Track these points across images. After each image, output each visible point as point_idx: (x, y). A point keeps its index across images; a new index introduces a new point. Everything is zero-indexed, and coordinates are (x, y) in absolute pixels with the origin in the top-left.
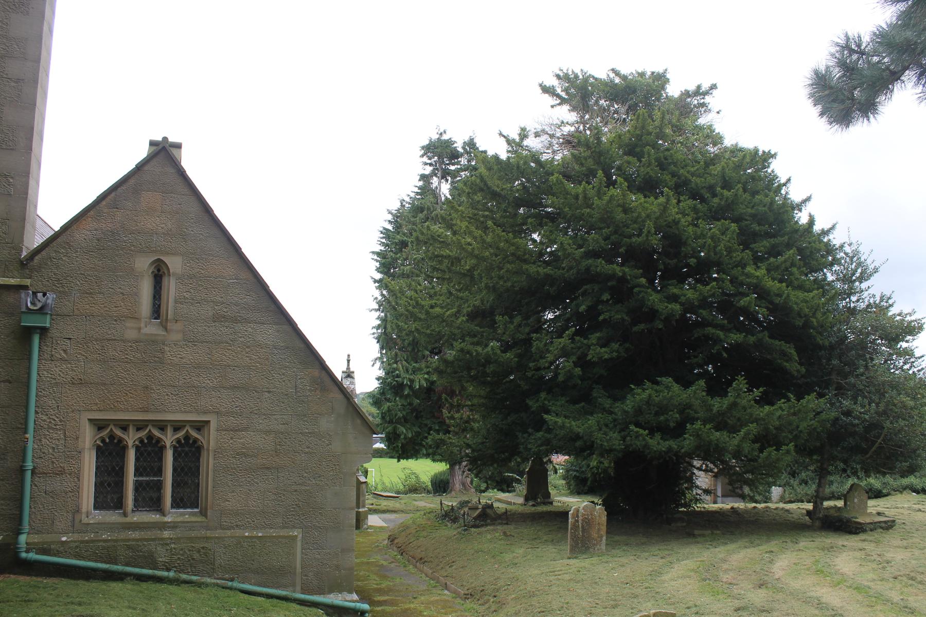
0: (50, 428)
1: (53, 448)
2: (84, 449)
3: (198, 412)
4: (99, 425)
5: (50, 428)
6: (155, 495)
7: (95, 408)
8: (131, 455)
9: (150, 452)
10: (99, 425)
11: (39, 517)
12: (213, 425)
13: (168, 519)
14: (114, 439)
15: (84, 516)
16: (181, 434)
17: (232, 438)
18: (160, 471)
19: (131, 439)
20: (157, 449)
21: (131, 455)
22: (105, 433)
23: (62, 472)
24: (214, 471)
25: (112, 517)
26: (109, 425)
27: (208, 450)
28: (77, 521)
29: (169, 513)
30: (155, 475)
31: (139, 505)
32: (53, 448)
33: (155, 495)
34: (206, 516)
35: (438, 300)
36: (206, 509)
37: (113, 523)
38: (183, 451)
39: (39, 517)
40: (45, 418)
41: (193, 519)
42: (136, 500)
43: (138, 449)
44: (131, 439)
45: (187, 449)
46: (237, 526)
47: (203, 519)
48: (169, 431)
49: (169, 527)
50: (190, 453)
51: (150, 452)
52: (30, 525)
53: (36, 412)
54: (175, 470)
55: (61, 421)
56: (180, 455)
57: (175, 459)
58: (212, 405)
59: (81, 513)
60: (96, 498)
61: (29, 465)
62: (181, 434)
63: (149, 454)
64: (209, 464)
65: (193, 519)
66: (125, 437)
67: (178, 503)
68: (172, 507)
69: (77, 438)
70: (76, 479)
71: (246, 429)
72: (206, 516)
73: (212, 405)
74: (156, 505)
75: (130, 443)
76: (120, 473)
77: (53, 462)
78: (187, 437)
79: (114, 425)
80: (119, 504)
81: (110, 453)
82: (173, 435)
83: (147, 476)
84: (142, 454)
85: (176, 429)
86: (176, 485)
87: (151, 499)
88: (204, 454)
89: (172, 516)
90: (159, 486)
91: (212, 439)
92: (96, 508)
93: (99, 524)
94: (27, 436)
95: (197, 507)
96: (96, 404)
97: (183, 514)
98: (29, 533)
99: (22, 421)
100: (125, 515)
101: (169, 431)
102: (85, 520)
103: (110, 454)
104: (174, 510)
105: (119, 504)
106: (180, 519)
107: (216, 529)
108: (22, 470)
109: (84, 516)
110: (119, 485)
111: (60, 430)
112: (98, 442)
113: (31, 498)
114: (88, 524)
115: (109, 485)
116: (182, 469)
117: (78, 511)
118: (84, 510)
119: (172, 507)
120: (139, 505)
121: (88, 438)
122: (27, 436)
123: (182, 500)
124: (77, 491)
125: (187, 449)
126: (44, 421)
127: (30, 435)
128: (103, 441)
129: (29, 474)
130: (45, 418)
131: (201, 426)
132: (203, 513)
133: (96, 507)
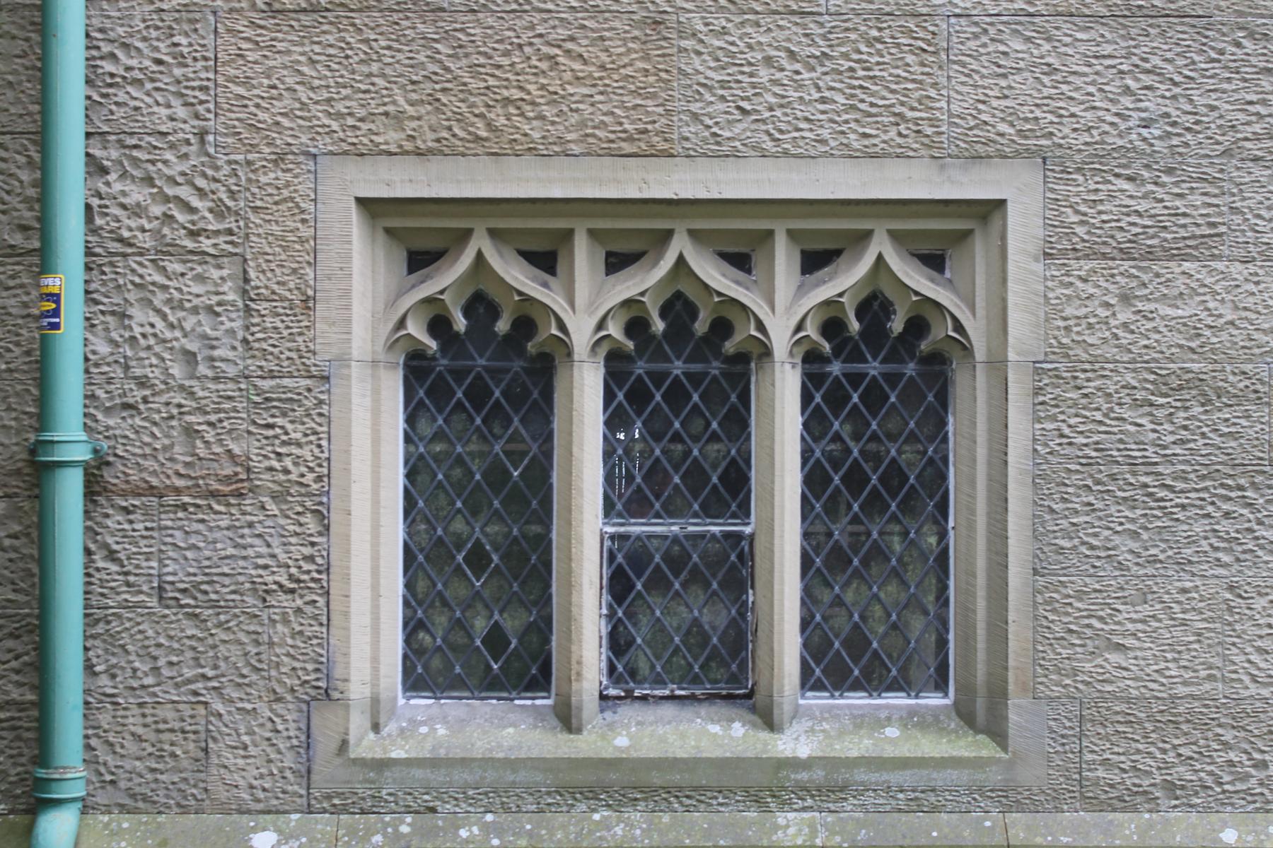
0: (167, 250)
1: (190, 357)
2: (343, 360)
3: (936, 155)
4: (417, 234)
5: (167, 250)
6: (715, 618)
7: (391, 138)
8: (585, 395)
9: (683, 380)
10: (417, 234)
11: (133, 722)
12: (1023, 227)
13: (794, 743)
14: (494, 312)
15: (358, 722)
16: (844, 281)
17: (1126, 299)
18: (734, 488)
19: (585, 307)
20: (715, 368)
21: (585, 395)
22: (447, 279)
23: (236, 488)
24: (1038, 480)
25: (501, 729)
26: (464, 236)
27: (998, 365)
28: (325, 744)
29: (796, 713)
30: (711, 510)
31: (633, 669)
32: (190, 357)
33: (715, 618)
34: (997, 732)
35: (229, 712)
36: (998, 694)
37: (511, 764)
38: (855, 379)
39: (133, 722)
40: (137, 194)
41: (930, 746)
42: (618, 643)
43: (616, 366)
44: (585, 307)
45: (874, 368)
46: (1170, 787)
47: (984, 748)
48: (584, 259)
49: (803, 790)
50: (892, 376)
51: (683, 380)
52: (91, 762)
53: (96, 167)
54: (814, 480)
55: (219, 211)
56: (837, 399)
57: (814, 424)
58: (1010, 116)
59: (345, 704)
60: (412, 627)
61: (72, 438)
62: (844, 281)
63: (677, 395)
64: (1003, 445)
65: (930, 746)
66: (552, 297)
67: (831, 665)
68: (808, 681)
69: (308, 303)
70: (312, 525)
71: (1202, 246)
72: (997, 732)
73: (1010, 116)
74: (722, 669)
75: (581, 332)
76: (530, 494)
77: (191, 432)
78: (874, 306)
79: (494, 233)
80: (526, 666)
81: (477, 382)
82: (801, 290)
83: (670, 511)
84: (639, 396)
85: (816, 261)
86: (823, 563)
87: (696, 634)
88: (971, 396)
89: (817, 728)
90: (735, 568)
91: (1017, 307)
92: (414, 682)
93: (433, 763)
94: (52, 283)
95: (941, 684)
96: (398, 119)
97: (876, 722)
98: (87, 807)
99: (28, 216)
100: (567, 719)
101: (584, 259)
102: (366, 746)
103: (478, 394)
104: (817, 701)
105: (526, 666)
106: (857, 746)
107: (1054, 801)
108: (38, 470)
109: (358, 722)
110: (530, 567)
111: (217, 258)
112: (416, 330)
113: (90, 620)
114: (382, 765)
115: (478, 559)
116: (855, 480)
117: (324, 692)
118: (358, 690)
119: (808, 681)
120: (633, 669)
121: (363, 308)
122: (52, 283)
123: (857, 642)
124: (316, 583)
125: (874, 368)
126: (137, 211)
127: (68, 278)
128: (439, 325)
129: (69, 491)
130: (137, 194)
131: (948, 232)
132: (983, 714)
133: (414, 682)
